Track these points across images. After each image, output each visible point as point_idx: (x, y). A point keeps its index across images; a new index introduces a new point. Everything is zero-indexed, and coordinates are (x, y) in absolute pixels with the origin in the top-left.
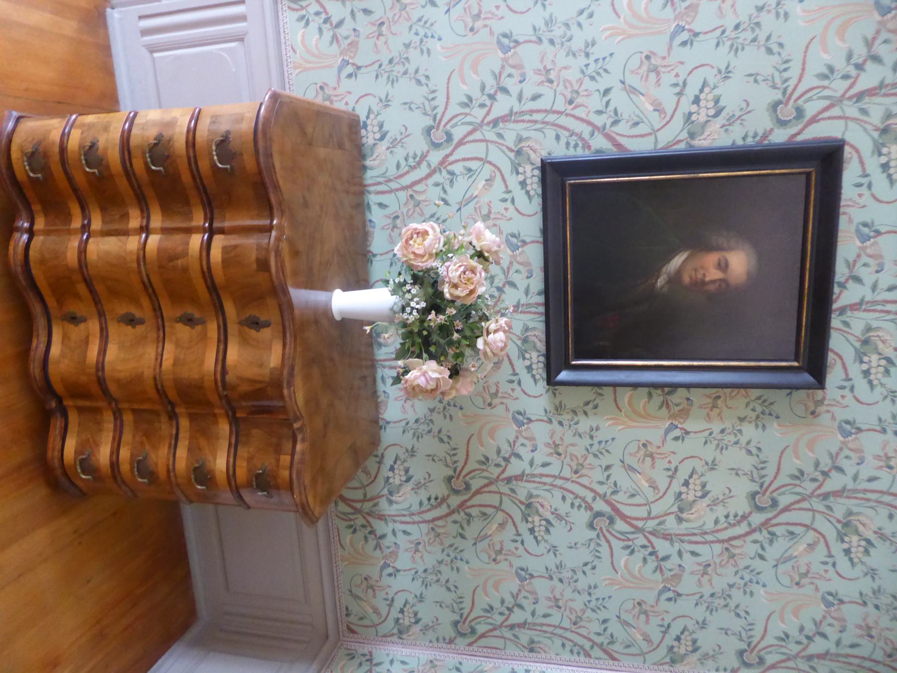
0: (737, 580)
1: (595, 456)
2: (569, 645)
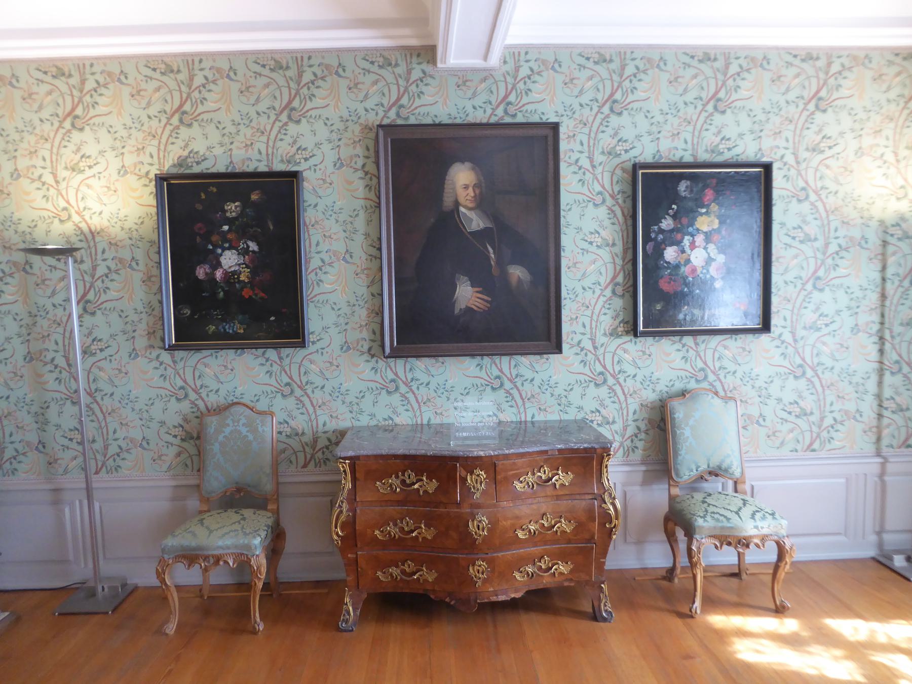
1: (251, 121)
2: (807, 125)
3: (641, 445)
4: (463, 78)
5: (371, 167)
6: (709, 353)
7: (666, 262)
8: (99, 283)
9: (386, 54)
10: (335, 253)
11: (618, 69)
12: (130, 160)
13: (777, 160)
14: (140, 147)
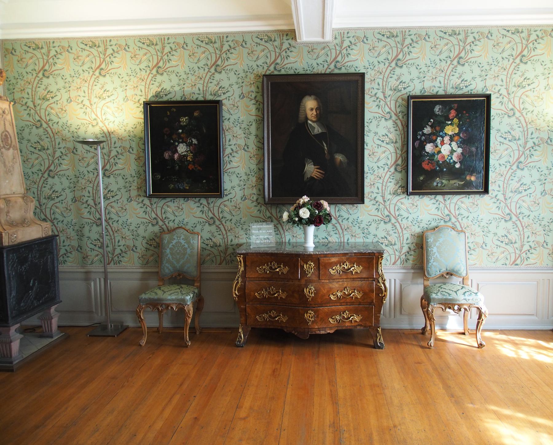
0: (238, 127)
2: (44, 185)
3: (411, 258)
4: (311, 48)
5: (259, 98)
6: (452, 206)
7: (427, 153)
8: (112, 160)
9: (269, 34)
10: (239, 146)
11: (401, 42)
12: (130, 93)
13: (495, 93)
14: (135, 86)
